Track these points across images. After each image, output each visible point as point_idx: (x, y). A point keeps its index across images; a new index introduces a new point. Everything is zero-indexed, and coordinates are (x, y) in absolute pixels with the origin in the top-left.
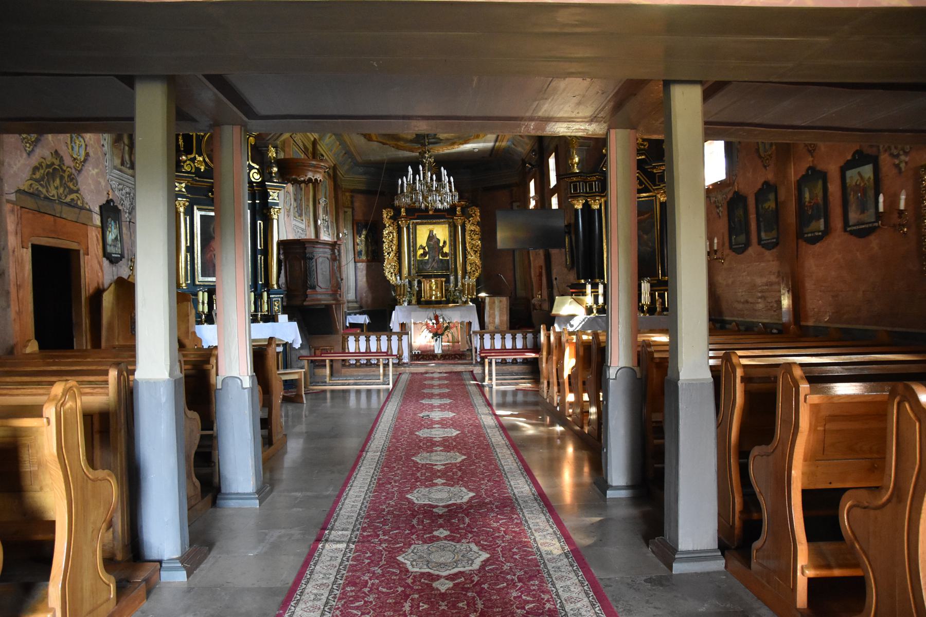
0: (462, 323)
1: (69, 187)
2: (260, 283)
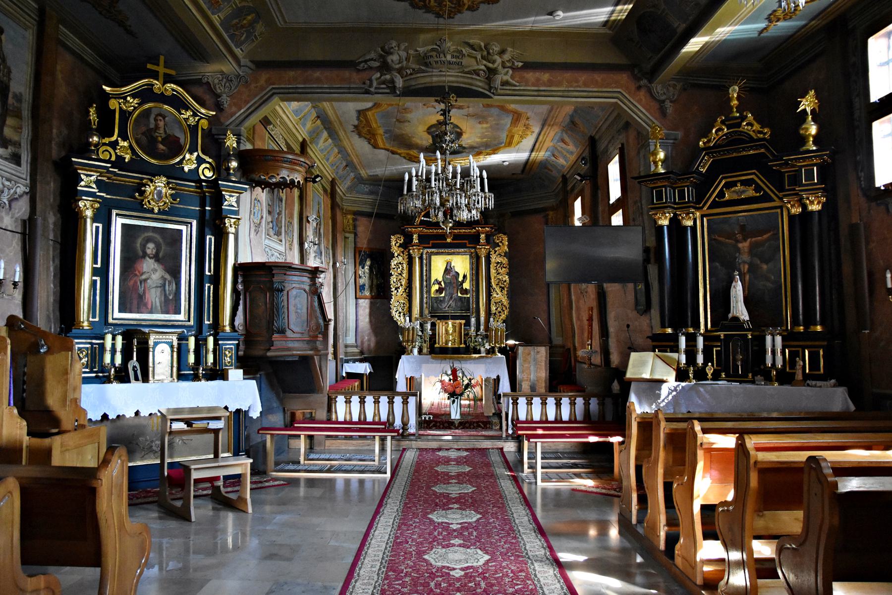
0: (487, 380)
2: (207, 322)
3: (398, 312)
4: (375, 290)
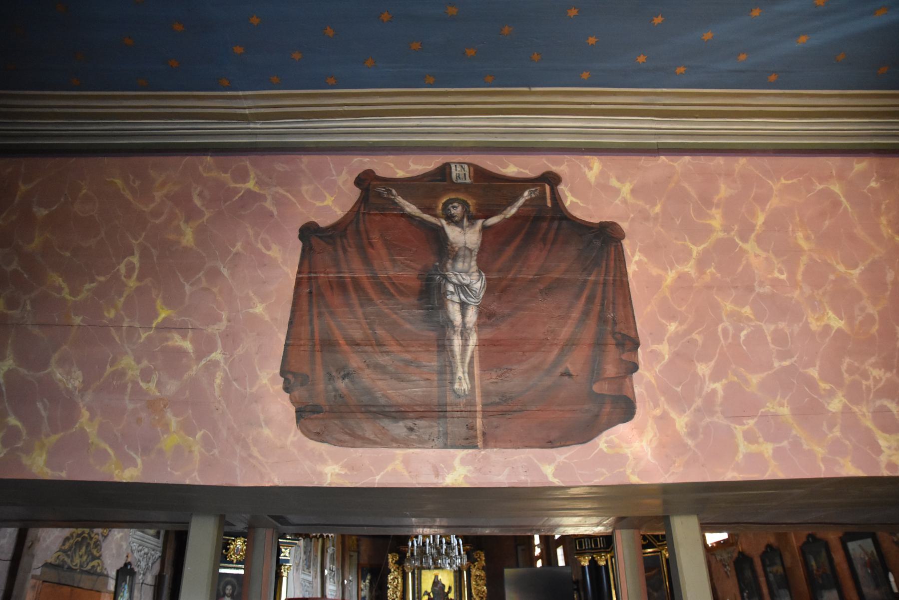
1: (92, 554)
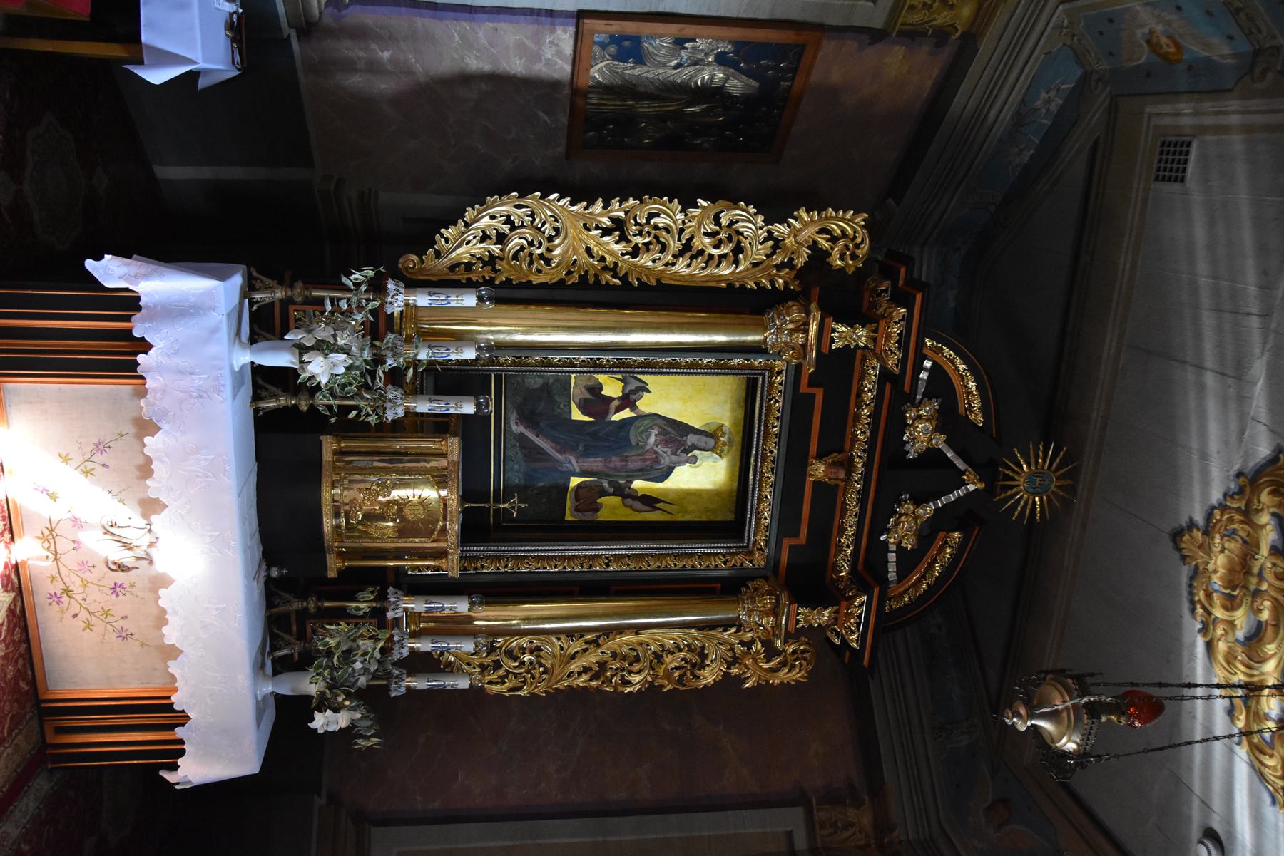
3: (505, 228)
4: (612, 105)
